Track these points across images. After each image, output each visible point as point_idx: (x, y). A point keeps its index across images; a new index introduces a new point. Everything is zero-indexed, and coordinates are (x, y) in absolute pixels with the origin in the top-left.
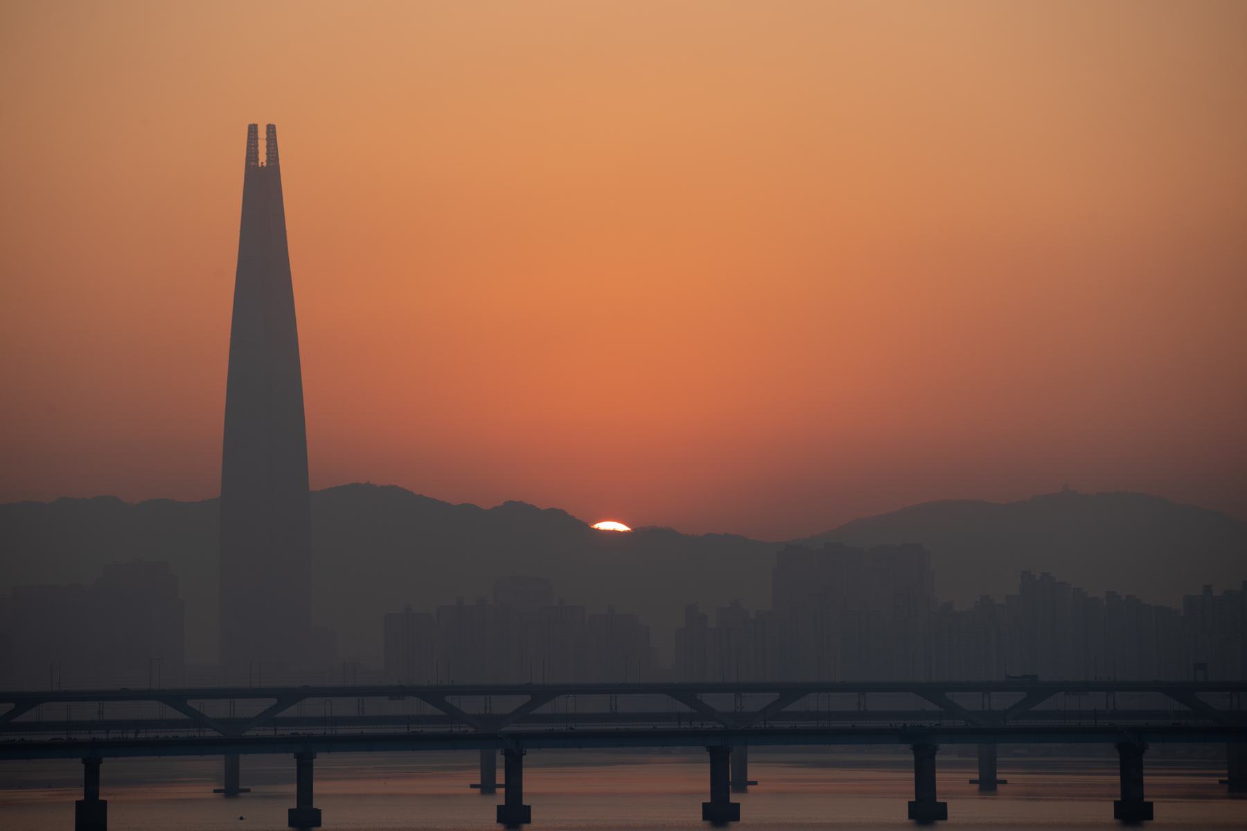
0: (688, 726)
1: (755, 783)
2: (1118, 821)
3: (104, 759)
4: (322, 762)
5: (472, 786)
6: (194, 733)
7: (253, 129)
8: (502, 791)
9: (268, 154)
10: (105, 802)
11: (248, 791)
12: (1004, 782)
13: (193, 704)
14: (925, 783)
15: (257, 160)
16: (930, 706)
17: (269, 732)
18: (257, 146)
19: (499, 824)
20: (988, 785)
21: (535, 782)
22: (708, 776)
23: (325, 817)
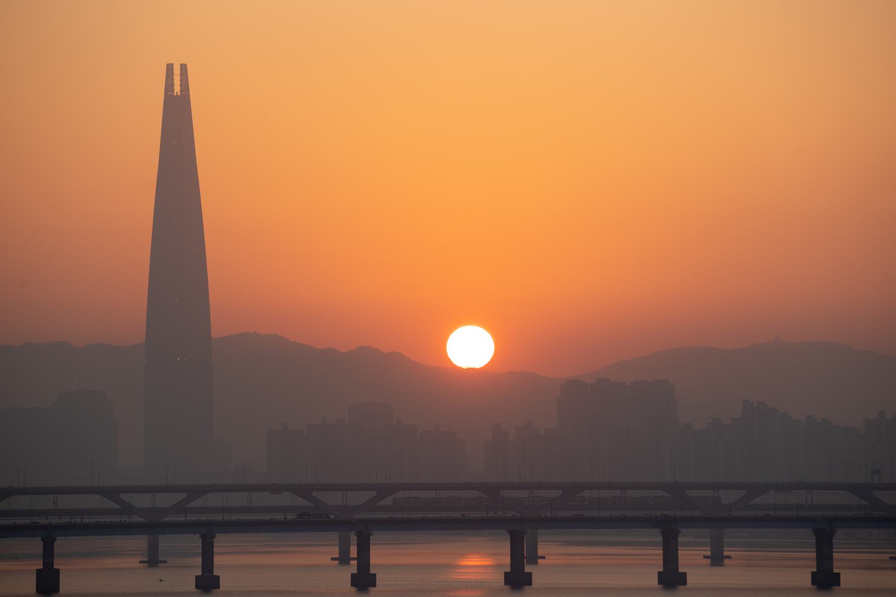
7: (170, 68)
15: (173, 90)
18: (173, 80)
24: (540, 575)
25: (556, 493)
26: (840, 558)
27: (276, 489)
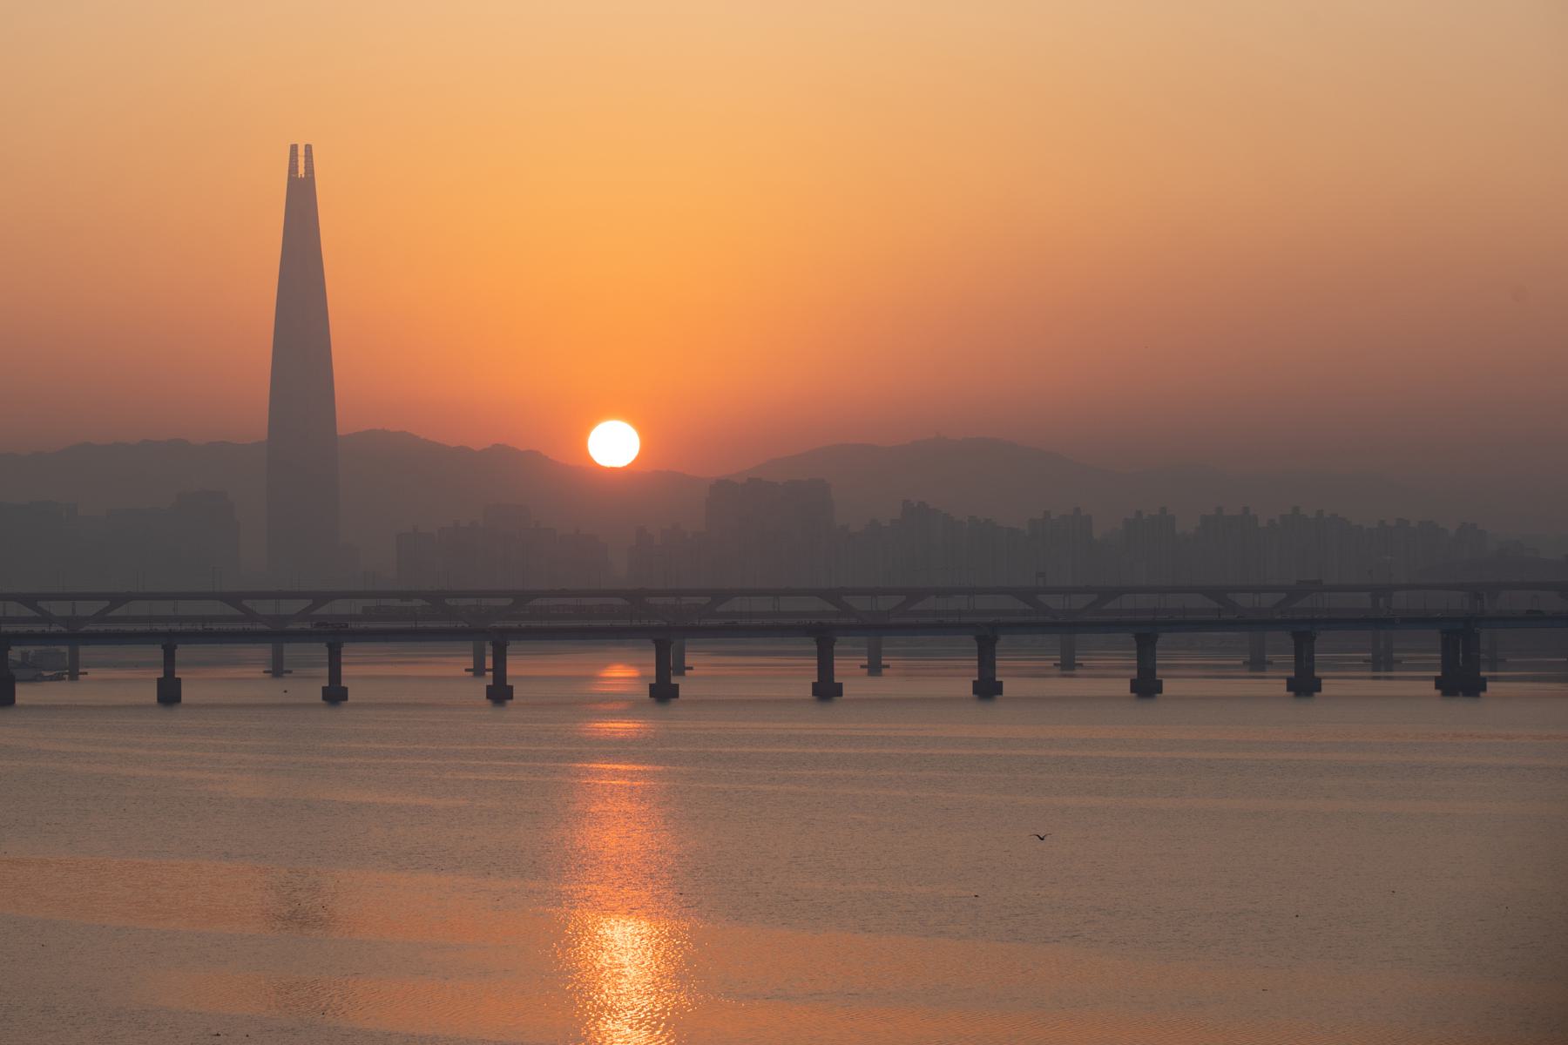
0: (639, 624)
1: (691, 668)
2: (815, 697)
3: (179, 646)
4: (349, 651)
5: (467, 670)
6: (248, 626)
7: (294, 148)
8: (491, 673)
9: (305, 168)
10: (179, 680)
11: (290, 672)
12: (888, 666)
13: (42, 604)
14: (825, 668)
15: (297, 172)
16: (831, 608)
17: (102, 628)
18: (297, 161)
19: (489, 701)
20: (875, 668)
21: (517, 667)
22: (654, 661)
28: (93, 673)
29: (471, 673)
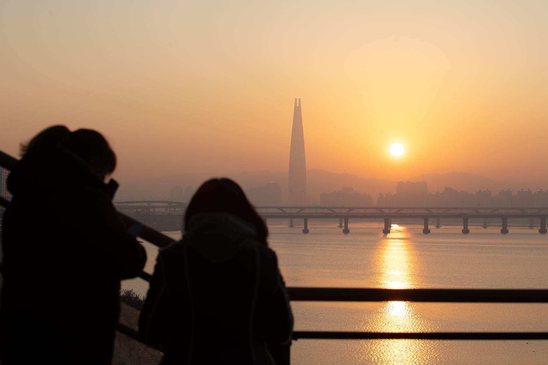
7: (296, 99)
15: (297, 105)
18: (297, 102)
23: (470, 231)
24: (511, 230)
25: (167, 204)
26: (350, 226)
27: (323, 208)
28: (443, 227)
29: (435, 227)
